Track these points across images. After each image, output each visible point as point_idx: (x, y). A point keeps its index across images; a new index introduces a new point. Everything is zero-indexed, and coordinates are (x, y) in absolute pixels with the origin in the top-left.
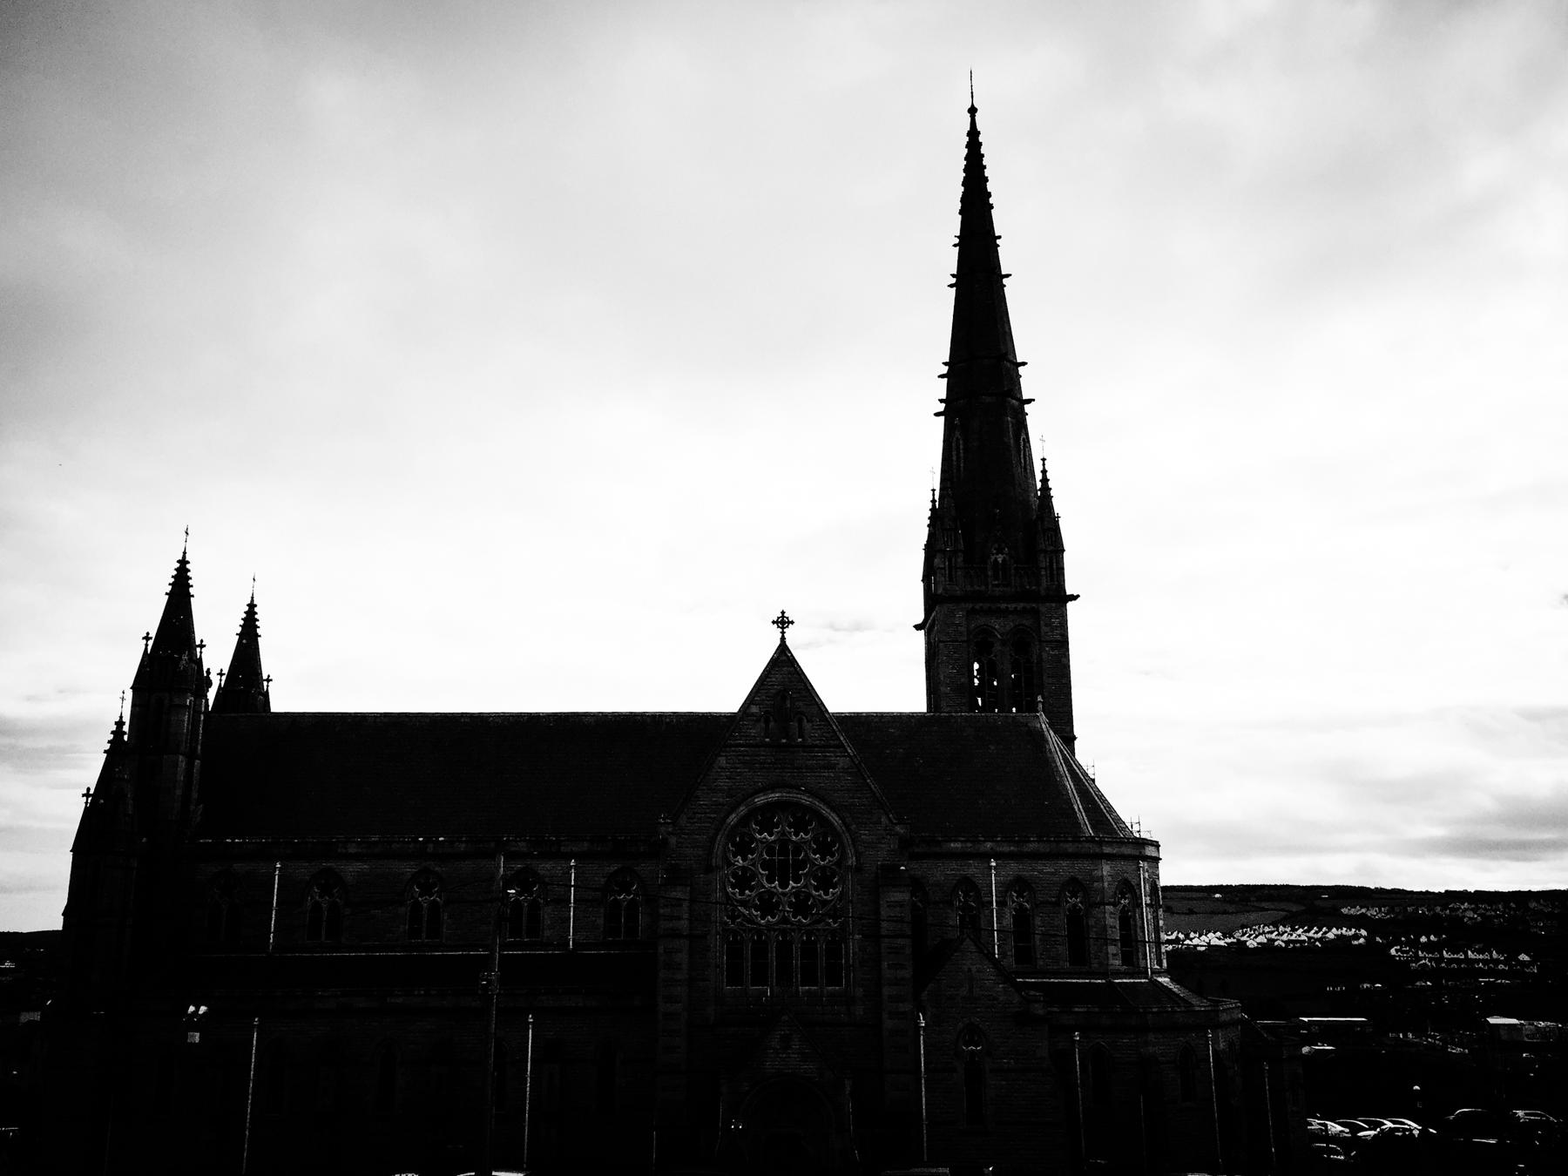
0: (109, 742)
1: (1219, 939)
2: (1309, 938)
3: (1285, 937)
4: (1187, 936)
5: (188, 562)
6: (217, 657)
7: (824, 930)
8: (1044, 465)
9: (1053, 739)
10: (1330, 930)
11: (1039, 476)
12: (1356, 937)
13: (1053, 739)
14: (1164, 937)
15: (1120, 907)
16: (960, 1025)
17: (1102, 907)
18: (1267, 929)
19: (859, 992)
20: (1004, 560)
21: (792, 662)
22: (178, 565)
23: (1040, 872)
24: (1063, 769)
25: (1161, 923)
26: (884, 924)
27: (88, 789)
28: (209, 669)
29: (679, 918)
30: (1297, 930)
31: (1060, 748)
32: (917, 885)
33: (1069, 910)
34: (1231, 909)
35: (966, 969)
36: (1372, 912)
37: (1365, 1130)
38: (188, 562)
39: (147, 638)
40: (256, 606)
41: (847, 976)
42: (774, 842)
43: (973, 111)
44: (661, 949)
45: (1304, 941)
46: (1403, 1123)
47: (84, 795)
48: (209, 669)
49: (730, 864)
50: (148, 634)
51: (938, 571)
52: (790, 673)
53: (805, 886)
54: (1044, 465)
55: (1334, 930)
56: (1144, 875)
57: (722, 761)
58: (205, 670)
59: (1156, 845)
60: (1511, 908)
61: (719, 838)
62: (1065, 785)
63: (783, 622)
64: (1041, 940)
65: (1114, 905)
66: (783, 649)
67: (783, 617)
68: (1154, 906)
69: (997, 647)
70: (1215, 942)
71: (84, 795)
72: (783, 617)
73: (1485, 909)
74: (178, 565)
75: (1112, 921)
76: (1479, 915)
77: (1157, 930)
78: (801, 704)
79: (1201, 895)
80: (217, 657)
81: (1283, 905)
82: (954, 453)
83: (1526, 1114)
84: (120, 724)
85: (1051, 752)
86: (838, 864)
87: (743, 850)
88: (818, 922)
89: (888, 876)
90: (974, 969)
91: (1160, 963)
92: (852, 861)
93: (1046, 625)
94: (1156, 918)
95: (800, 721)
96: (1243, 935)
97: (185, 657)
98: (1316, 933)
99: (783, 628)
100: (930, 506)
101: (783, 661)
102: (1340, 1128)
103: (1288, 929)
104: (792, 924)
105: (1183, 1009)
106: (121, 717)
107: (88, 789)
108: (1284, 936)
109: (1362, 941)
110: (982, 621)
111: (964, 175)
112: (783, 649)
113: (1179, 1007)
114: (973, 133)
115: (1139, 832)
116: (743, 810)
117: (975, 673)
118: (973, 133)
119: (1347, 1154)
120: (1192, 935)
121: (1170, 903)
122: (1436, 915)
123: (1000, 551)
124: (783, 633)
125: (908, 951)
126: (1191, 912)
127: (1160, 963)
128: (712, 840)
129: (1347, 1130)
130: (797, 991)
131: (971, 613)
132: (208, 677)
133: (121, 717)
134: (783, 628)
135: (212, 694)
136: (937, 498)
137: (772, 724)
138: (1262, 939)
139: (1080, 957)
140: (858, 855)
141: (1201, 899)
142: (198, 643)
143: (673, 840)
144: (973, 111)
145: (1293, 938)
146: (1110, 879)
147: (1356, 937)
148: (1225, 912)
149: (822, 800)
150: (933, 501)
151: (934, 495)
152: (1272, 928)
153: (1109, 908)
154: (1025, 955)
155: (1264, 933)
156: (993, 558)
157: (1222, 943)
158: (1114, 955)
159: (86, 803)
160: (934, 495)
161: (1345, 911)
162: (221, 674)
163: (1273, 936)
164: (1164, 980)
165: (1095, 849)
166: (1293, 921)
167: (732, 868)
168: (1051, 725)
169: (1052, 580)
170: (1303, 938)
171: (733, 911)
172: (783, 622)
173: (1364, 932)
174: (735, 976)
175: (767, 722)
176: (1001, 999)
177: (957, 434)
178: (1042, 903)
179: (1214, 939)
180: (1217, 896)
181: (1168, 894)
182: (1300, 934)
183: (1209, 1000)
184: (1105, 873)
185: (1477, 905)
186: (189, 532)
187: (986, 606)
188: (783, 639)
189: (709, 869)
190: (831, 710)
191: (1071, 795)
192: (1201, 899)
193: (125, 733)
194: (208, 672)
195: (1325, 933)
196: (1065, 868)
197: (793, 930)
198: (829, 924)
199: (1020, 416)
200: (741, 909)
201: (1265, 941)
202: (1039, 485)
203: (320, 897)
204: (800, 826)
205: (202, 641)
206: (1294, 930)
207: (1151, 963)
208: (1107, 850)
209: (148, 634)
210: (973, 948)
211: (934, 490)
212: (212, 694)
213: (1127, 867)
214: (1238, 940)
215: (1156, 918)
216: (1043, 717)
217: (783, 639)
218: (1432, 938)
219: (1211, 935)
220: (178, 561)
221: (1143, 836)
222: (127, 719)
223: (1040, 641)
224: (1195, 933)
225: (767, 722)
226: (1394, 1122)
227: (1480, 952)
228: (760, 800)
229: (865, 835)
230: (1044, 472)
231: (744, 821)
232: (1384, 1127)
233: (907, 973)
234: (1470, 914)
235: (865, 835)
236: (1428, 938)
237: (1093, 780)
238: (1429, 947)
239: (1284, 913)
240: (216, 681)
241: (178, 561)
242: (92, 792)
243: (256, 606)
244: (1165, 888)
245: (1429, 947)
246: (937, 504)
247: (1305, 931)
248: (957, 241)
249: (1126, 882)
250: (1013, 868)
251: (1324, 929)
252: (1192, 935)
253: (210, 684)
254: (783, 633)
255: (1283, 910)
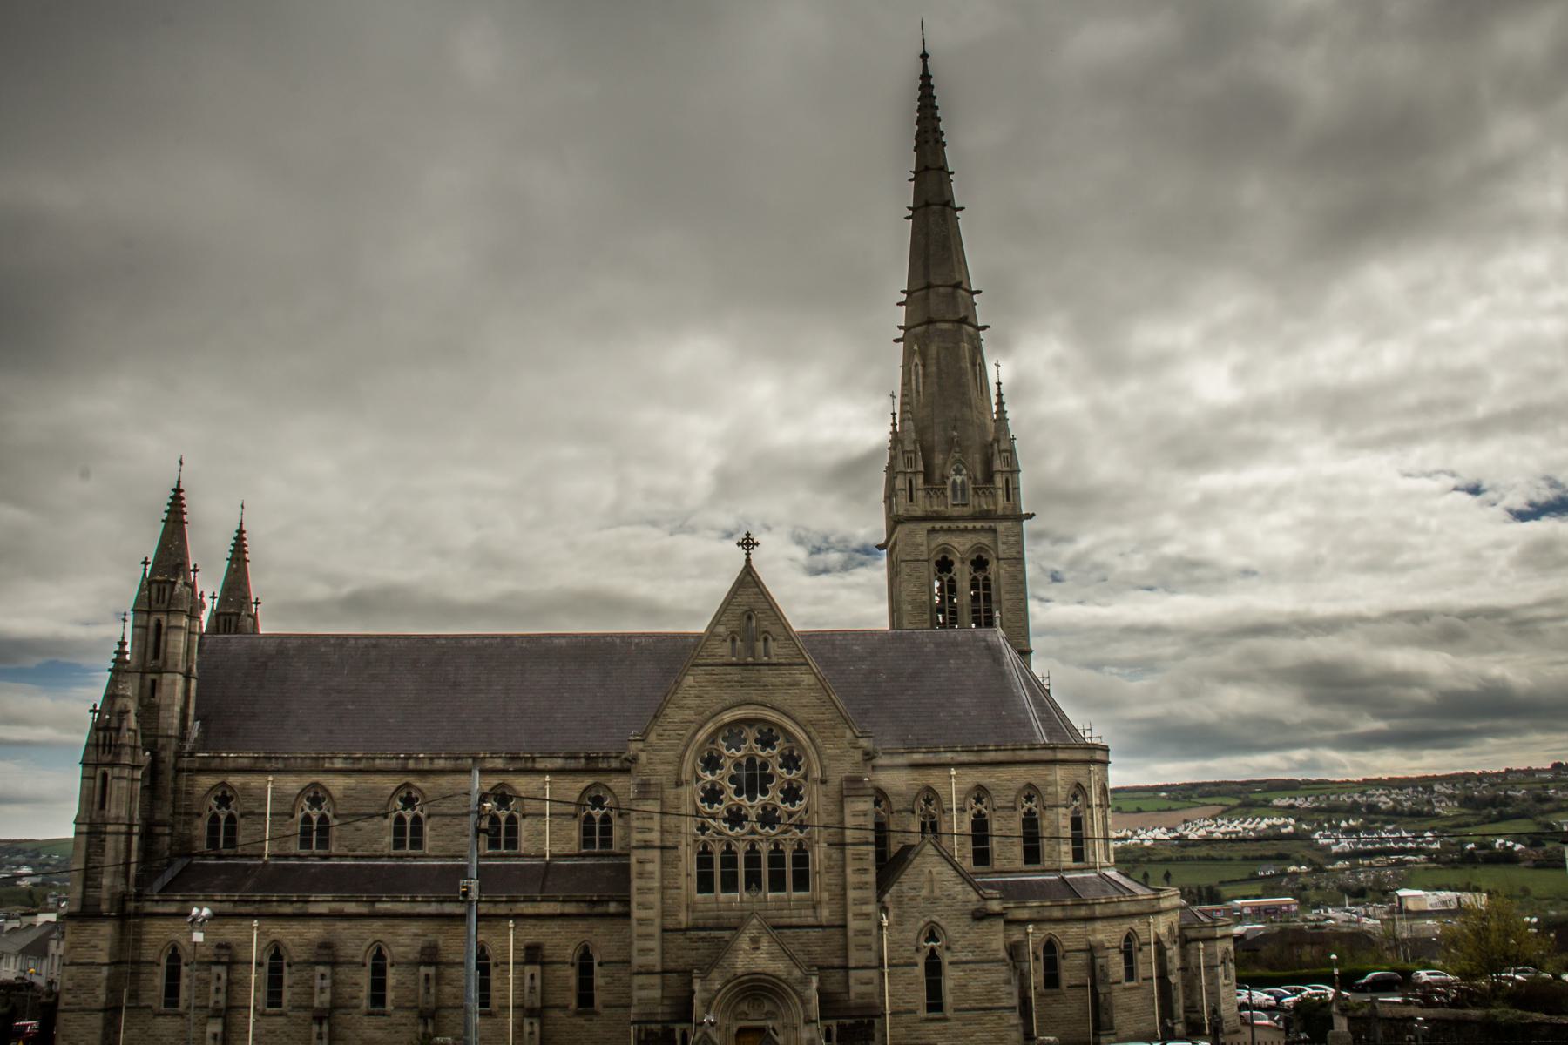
0: (113, 661)
1: (1164, 834)
2: (1244, 829)
3: (1223, 829)
4: (1135, 832)
5: (182, 491)
6: (209, 586)
7: (791, 839)
8: (999, 389)
9: (1009, 654)
10: (1262, 819)
11: (994, 400)
12: (1285, 826)
13: (1009, 654)
14: (1113, 834)
15: (1072, 808)
16: (922, 923)
17: (1055, 809)
18: (1207, 823)
19: (825, 896)
20: (963, 481)
21: (757, 583)
22: (173, 493)
23: (997, 779)
24: (1018, 680)
25: (1109, 821)
26: (848, 832)
27: (95, 706)
28: (202, 593)
29: (650, 830)
30: (1233, 822)
31: (1019, 667)
32: (880, 796)
33: (1025, 814)
34: (1174, 805)
35: (927, 871)
36: (1299, 802)
37: (1288, 996)
38: (182, 491)
39: (146, 563)
40: (244, 532)
41: (814, 881)
42: (742, 757)
43: (924, 56)
44: (633, 860)
45: (1239, 832)
46: (1321, 989)
47: (91, 711)
48: (202, 593)
49: (698, 779)
50: (146, 559)
51: (899, 493)
52: (756, 594)
53: (773, 798)
54: (999, 389)
55: (1266, 820)
56: (1094, 778)
57: (689, 680)
58: (199, 593)
59: (1106, 749)
60: (1418, 792)
61: (687, 755)
62: (1020, 696)
63: (748, 544)
64: (998, 842)
65: (1067, 807)
66: (748, 569)
67: (748, 538)
68: (1104, 806)
69: (957, 566)
70: (1160, 836)
71: (91, 711)
72: (748, 538)
73: (1397, 794)
74: (173, 493)
75: (1065, 823)
76: (1391, 799)
77: (1106, 829)
78: (766, 623)
79: (1147, 794)
80: (209, 586)
81: (1218, 800)
82: (913, 378)
83: (1428, 974)
84: (122, 644)
85: (1017, 688)
86: (805, 777)
87: (712, 763)
88: (786, 832)
89: (853, 786)
90: (935, 871)
91: (1108, 858)
92: (817, 774)
93: (1004, 543)
94: (1105, 817)
95: (766, 640)
96: (1185, 829)
97: (180, 581)
98: (1251, 823)
99: (748, 550)
100: (891, 429)
101: (748, 579)
102: (1266, 996)
103: (1226, 822)
104: (761, 834)
105: (1128, 899)
106: (123, 638)
107: (95, 706)
108: (1222, 828)
109: (1290, 829)
110: (941, 539)
111: (917, 128)
112: (748, 569)
113: (1124, 896)
114: (926, 77)
115: (1091, 738)
116: (710, 727)
117: (936, 591)
118: (926, 77)
119: (1271, 1018)
120: (1139, 832)
121: (1119, 804)
122: (1355, 802)
123: (958, 472)
124: (748, 554)
125: (872, 856)
126: (1139, 811)
127: (1108, 858)
128: (681, 757)
129: (1272, 998)
130: (765, 897)
131: (932, 531)
132: (201, 600)
133: (123, 638)
134: (748, 550)
135: (205, 616)
136: (897, 421)
137: (738, 643)
138: (1202, 832)
139: (1032, 854)
140: (823, 768)
141: (1147, 798)
142: (192, 567)
143: (643, 757)
144: (924, 56)
145: (1230, 829)
146: (1063, 782)
147: (1285, 826)
148: (1170, 809)
149: (785, 714)
150: (894, 425)
151: (894, 418)
152: (1211, 822)
153: (1062, 810)
154: (982, 856)
155: (1204, 826)
156: (951, 479)
157: (1166, 837)
158: (1066, 853)
159: (94, 718)
160: (894, 418)
161: (1276, 802)
162: (213, 597)
163: (1212, 829)
164: (1112, 873)
165: (1048, 755)
166: (1228, 812)
167: (701, 783)
168: (1008, 639)
169: (1008, 499)
170: (1239, 828)
171: (703, 824)
172: (748, 544)
173: (1292, 821)
174: (705, 884)
175: (733, 640)
176: (960, 897)
177: (917, 360)
178: (999, 808)
179: (1159, 833)
180: (1163, 794)
181: (1117, 796)
182: (1237, 826)
183: (1153, 889)
184: (1058, 778)
185: (1390, 791)
186: (178, 464)
187: (945, 525)
188: (748, 560)
189: (679, 784)
190: (796, 628)
191: (1027, 706)
192: (1147, 798)
193: (127, 653)
194: (202, 595)
195: (1259, 823)
196: (1021, 775)
197: (761, 840)
198: (794, 834)
199: (976, 342)
200: (711, 821)
201: (1205, 833)
202: (995, 409)
203: (311, 808)
204: (767, 742)
205: (195, 566)
206: (1231, 821)
207: (1100, 859)
208: (1061, 755)
209: (146, 559)
210: (934, 852)
211: (894, 414)
212: (205, 616)
213: (1078, 773)
214: (1181, 834)
215: (1105, 817)
216: (1000, 632)
217: (748, 560)
218: (1351, 822)
219: (1156, 831)
220: (173, 490)
221: (1095, 741)
222: (128, 640)
223: (998, 559)
224: (1142, 829)
225: (733, 640)
226: (1313, 988)
227: (1391, 832)
228: (728, 717)
229: (830, 750)
230: (1000, 395)
231: (712, 738)
232: (1304, 993)
233: (871, 877)
234: (1383, 799)
235: (830, 750)
236: (1347, 822)
237: (1048, 691)
238: (1349, 831)
239: (1221, 808)
240: (209, 605)
241: (173, 490)
242: (98, 708)
243: (244, 532)
244: (1114, 791)
245: (1349, 831)
246: (898, 427)
247: (1241, 823)
248: (913, 176)
249: (1079, 785)
250: (973, 777)
251: (1258, 820)
252: (1139, 832)
253: (203, 606)
254: (748, 554)
255: (1221, 805)
